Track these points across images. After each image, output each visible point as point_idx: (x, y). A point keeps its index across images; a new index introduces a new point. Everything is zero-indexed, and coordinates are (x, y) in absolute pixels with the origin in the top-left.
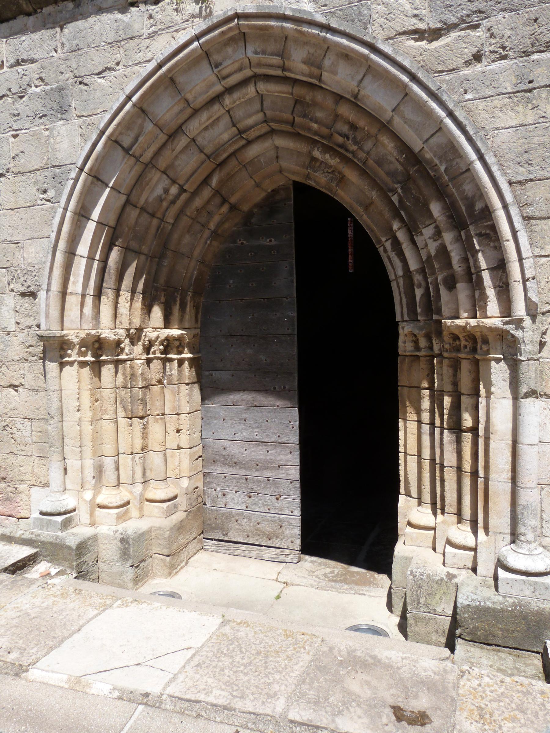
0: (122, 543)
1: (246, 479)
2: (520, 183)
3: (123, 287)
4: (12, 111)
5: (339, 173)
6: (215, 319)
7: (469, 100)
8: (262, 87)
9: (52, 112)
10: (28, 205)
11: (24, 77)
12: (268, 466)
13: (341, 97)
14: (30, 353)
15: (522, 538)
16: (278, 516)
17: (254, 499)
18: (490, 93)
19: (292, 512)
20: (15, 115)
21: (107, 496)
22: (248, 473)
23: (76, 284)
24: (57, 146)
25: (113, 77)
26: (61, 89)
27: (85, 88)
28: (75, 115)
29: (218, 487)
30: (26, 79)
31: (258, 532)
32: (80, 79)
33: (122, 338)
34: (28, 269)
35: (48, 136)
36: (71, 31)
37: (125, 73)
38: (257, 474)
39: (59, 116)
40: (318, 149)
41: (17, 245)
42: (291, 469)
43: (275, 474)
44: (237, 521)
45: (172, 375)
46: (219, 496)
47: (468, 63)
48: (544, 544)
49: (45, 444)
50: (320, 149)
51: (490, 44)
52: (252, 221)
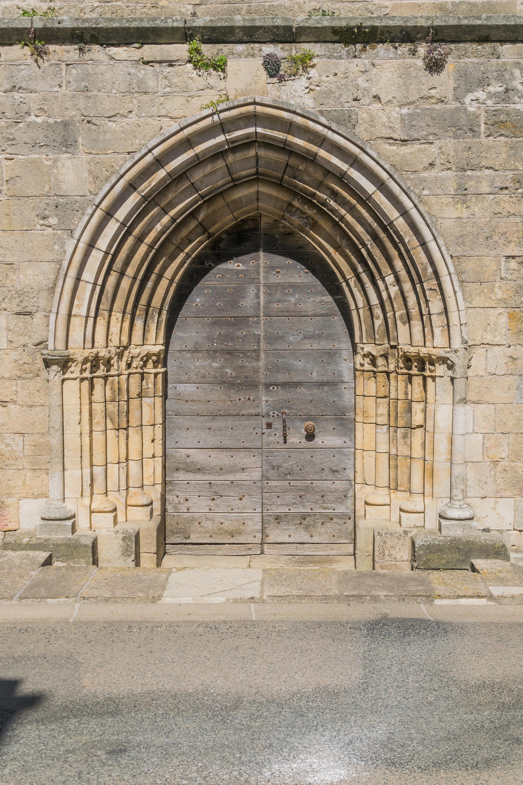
0: (124, 541)
1: (210, 483)
2: (458, 257)
3: (115, 308)
4: (7, 136)
5: (312, 219)
6: (181, 334)
7: (425, 195)
8: (262, 152)
9: (55, 144)
10: (25, 228)
11: (22, 105)
12: (232, 470)
13: (329, 172)
14: (25, 370)
15: (455, 498)
16: (241, 514)
17: (218, 501)
18: (440, 193)
19: (255, 510)
20: (8, 139)
21: (98, 502)
22: (212, 478)
23: (81, 308)
24: (61, 178)
25: (124, 123)
26: (66, 125)
27: (94, 127)
28: (82, 151)
29: (178, 493)
30: (25, 108)
31: (221, 531)
32: (89, 119)
33: (113, 356)
34: (25, 290)
35: (50, 166)
36: (80, 72)
37: (138, 122)
38: (221, 478)
39: (64, 149)
40: (298, 200)
41: (10, 266)
42: (254, 471)
43: (238, 477)
44: (200, 523)
45: (148, 388)
46: (181, 502)
47: (425, 169)
48: (468, 502)
49: (40, 457)
50: (300, 201)
51: (441, 159)
52: (221, 245)
